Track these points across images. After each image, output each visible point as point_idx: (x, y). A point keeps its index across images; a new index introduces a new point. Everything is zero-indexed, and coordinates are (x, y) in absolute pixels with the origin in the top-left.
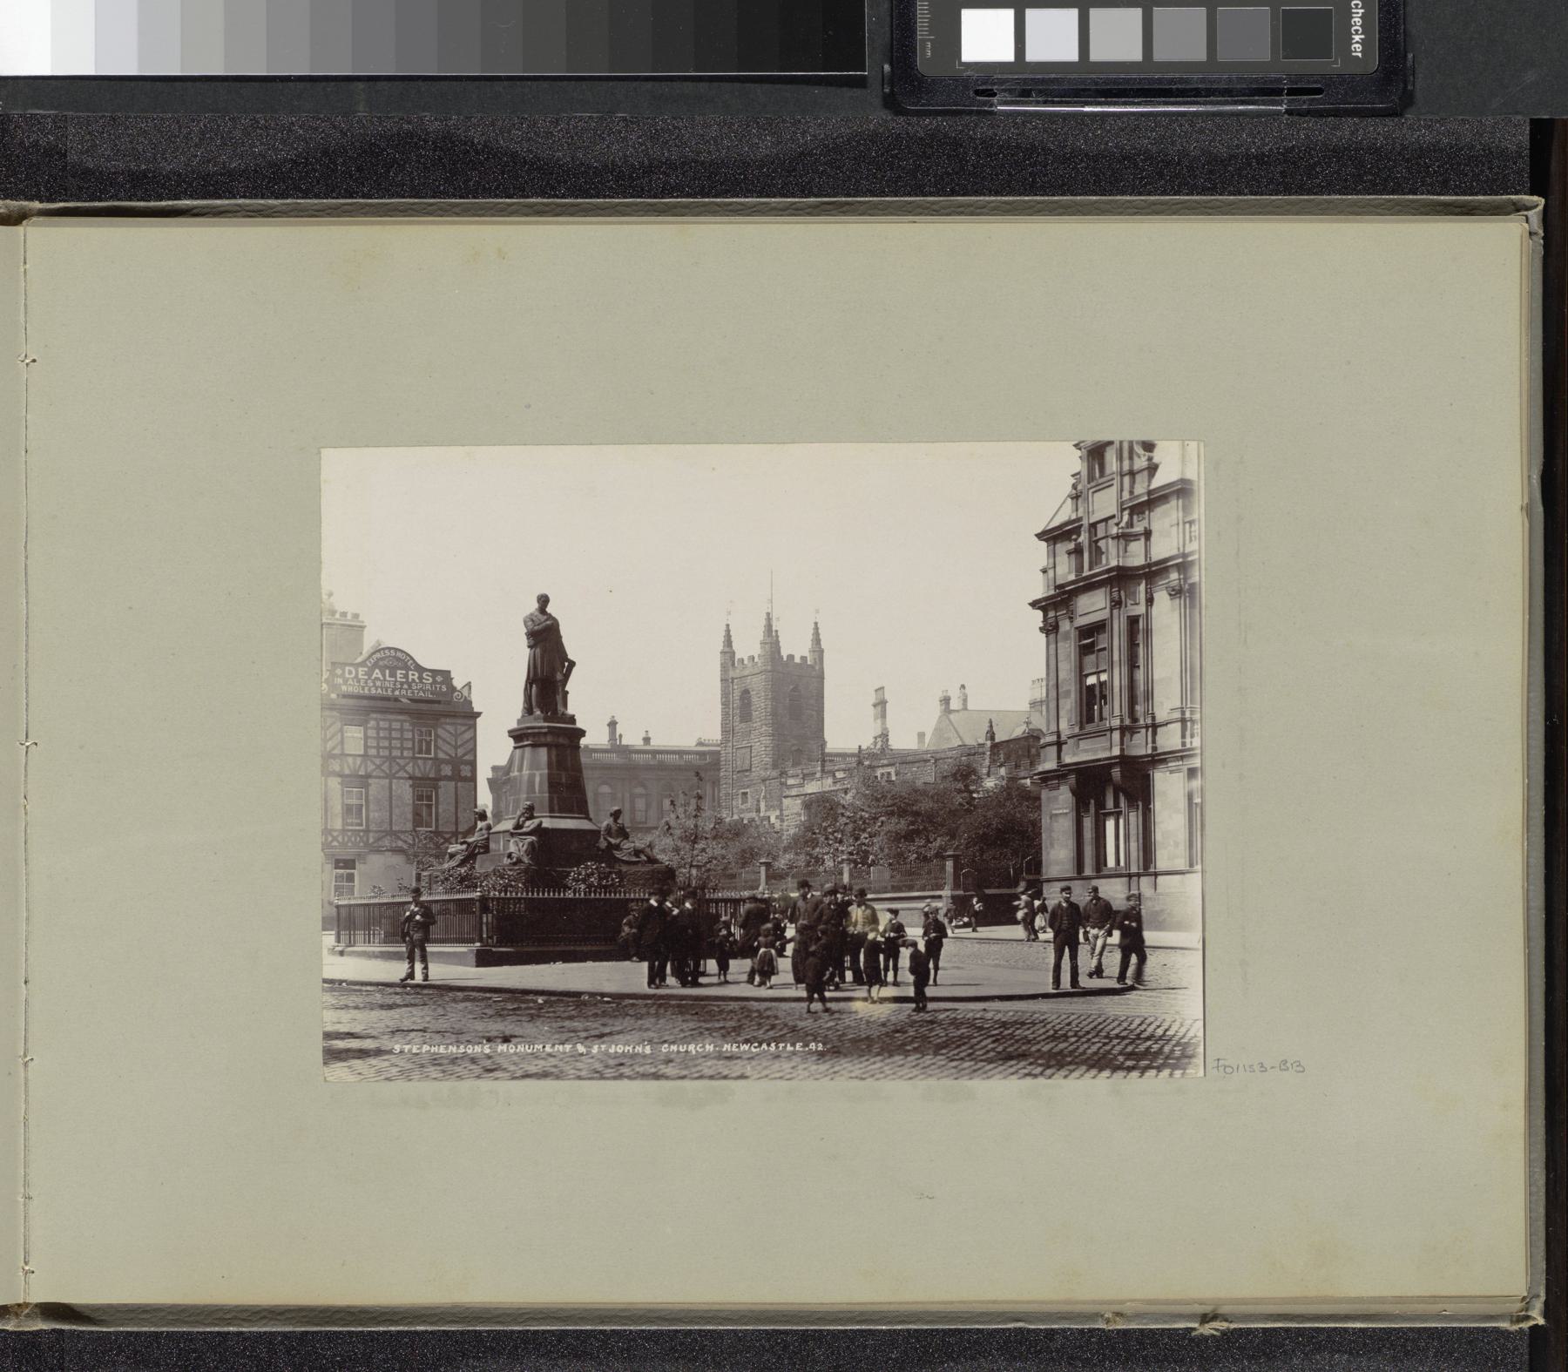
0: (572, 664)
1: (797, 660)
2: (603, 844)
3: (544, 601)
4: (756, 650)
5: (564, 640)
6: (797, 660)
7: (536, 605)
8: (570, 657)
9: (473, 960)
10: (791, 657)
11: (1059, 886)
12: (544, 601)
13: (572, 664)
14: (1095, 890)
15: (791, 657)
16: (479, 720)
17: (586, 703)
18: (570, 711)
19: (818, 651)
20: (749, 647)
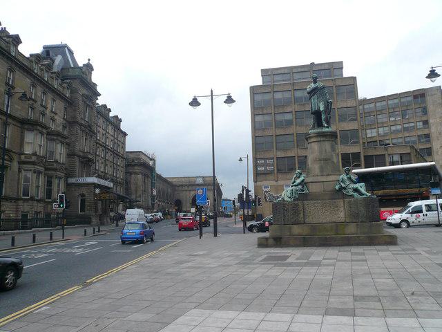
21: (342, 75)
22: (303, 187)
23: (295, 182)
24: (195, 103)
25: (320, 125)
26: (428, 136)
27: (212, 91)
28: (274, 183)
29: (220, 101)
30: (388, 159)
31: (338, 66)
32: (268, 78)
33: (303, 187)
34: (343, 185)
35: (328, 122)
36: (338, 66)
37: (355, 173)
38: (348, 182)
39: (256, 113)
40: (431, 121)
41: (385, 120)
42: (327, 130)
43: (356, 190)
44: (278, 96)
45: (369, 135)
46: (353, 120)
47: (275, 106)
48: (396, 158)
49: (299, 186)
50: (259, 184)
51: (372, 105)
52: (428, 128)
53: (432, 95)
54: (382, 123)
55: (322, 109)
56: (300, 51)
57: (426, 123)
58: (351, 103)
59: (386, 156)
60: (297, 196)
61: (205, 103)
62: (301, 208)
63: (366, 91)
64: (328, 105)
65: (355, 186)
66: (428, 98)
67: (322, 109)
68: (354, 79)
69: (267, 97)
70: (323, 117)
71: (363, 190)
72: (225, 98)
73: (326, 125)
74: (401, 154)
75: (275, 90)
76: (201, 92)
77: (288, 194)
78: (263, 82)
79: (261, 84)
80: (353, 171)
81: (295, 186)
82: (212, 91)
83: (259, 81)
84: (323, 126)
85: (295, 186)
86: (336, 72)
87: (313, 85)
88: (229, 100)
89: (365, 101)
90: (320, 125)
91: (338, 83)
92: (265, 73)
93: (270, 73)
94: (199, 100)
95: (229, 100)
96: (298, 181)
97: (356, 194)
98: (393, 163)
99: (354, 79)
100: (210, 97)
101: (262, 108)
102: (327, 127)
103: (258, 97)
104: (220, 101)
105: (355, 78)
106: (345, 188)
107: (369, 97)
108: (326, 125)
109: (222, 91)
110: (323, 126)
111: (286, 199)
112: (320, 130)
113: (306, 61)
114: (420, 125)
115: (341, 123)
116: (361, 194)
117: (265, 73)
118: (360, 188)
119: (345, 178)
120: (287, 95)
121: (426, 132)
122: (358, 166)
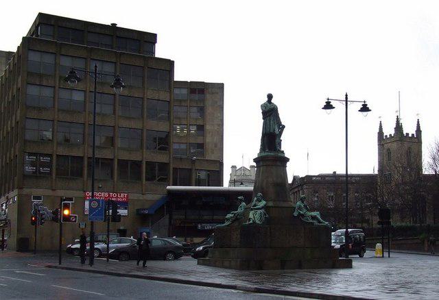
0: (284, 127)
1: (410, 136)
2: (296, 214)
3: (270, 97)
4: (393, 132)
5: (280, 116)
6: (410, 136)
7: (267, 99)
8: (283, 123)
9: (21, 236)
10: (407, 134)
11: (96, 152)
12: (270, 97)
13: (284, 127)
14: (434, 223)
15: (407, 134)
16: (288, 164)
17: (288, 144)
18: (282, 149)
19: (419, 131)
20: (389, 130)
24: (328, 106)
26: (201, 146)
27: (346, 95)
28: (49, 192)
29: (354, 108)
36: (150, 39)
40: (208, 127)
52: (203, 136)
53: (213, 93)
56: (159, 39)
57: (201, 128)
59: (193, 171)
61: (339, 107)
66: (208, 95)
72: (360, 106)
74: (209, 171)
76: (336, 95)
82: (346, 95)
83: (161, 52)
88: (365, 108)
93: (53, 23)
94: (333, 103)
95: (365, 108)
100: (344, 102)
101: (41, 76)
104: (354, 108)
106: (303, 216)
109: (357, 96)
113: (106, 21)
114: (193, 130)
121: (200, 140)
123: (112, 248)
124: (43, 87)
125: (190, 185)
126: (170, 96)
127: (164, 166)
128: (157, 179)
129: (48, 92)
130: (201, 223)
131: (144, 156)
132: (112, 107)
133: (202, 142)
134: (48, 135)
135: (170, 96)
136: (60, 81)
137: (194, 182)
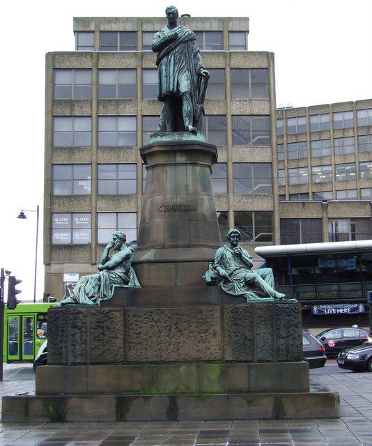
2: (208, 276)
21: (245, 46)
22: (127, 273)
23: (107, 259)
25: (178, 126)
30: (328, 229)
31: (239, 28)
32: (87, 39)
33: (127, 273)
34: (222, 271)
35: (195, 122)
36: (239, 28)
37: (260, 254)
38: (233, 265)
39: (58, 111)
41: (325, 152)
42: (192, 138)
43: (251, 284)
44: (107, 79)
45: (293, 181)
46: (260, 143)
47: (99, 102)
48: (344, 227)
49: (119, 271)
50: (55, 268)
51: (302, 121)
54: (321, 158)
55: (185, 86)
56: (169, 6)
58: (260, 108)
59: (325, 221)
60: (111, 294)
62: (119, 325)
63: (294, 89)
64: (201, 81)
65: (250, 274)
67: (185, 86)
68: (269, 56)
69: (84, 79)
70: (187, 107)
71: (268, 285)
73: (191, 127)
74: (352, 219)
75: (102, 64)
77: (89, 288)
78: (78, 47)
79: (71, 47)
80: (258, 249)
81: (109, 269)
83: (67, 42)
84: (185, 129)
85: (109, 269)
86: (236, 39)
87: (167, 32)
89: (290, 112)
90: (178, 126)
91: (237, 62)
92: (82, 26)
93: (92, 28)
96: (116, 257)
97: (252, 296)
98: (336, 237)
99: (269, 56)
101: (71, 103)
102: (194, 132)
103: (63, 79)
105: (273, 54)
106: (226, 280)
107: (295, 106)
108: (191, 127)
110: (185, 129)
111: (83, 299)
112: (175, 138)
115: (237, 147)
116: (262, 293)
117: (82, 26)
118: (260, 279)
119: (229, 255)
120: (128, 78)
122: (268, 239)
123: (223, 349)
124: (76, 119)
125: (297, 242)
126: (270, 107)
127: (266, 217)
128: (255, 238)
129: (82, 125)
130: (317, 304)
131: (231, 204)
132: (100, 129)
133: (218, 161)
134: (86, 187)
135: (270, 107)
136: (98, 106)
137: (326, 236)
